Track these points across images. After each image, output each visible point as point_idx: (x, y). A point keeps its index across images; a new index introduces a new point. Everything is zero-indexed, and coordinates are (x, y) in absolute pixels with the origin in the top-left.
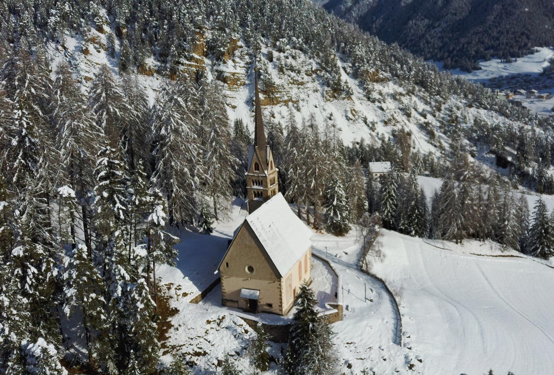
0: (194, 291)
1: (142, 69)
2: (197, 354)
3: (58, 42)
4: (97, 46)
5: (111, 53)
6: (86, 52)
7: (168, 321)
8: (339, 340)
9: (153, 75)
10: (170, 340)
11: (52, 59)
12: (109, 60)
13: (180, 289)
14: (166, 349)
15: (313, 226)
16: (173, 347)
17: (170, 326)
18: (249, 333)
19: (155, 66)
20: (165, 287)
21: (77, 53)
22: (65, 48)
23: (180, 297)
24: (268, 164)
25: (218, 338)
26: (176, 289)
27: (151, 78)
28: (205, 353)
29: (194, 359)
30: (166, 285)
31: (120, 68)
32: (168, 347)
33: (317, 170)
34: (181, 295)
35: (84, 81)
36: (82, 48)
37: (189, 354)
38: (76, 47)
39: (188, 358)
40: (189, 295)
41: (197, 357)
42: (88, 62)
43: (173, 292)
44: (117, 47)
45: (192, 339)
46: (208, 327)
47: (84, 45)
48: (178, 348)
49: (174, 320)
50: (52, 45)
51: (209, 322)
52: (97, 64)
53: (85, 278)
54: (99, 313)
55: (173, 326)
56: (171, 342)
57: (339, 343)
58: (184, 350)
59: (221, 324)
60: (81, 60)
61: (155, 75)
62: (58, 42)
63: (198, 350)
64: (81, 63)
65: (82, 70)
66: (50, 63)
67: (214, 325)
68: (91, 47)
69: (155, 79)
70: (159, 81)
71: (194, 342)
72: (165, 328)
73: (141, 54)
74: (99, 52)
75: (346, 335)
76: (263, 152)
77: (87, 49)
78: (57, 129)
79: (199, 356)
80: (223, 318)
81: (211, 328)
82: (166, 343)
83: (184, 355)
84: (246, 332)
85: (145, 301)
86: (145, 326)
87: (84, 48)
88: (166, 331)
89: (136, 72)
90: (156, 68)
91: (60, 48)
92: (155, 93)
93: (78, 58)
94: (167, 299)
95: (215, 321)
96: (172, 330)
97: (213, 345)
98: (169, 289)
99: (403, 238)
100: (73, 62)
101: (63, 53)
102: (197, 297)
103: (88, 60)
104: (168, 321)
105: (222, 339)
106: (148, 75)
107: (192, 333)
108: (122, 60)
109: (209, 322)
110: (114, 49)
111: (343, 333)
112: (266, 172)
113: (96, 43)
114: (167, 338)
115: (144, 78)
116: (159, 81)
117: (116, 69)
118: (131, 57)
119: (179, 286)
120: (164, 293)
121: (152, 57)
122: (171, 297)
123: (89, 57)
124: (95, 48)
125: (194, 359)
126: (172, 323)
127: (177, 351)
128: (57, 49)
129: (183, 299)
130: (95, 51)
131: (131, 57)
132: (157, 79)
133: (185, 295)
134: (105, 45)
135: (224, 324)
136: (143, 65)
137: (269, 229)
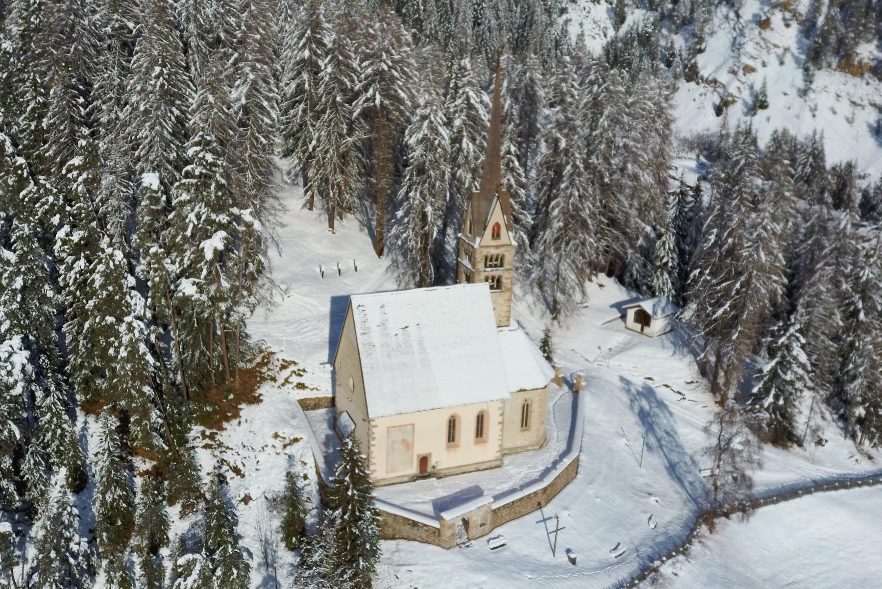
0: (323, 390)
1: (848, 64)
2: (237, 471)
3: (733, 5)
4: (788, 15)
5: (808, 28)
6: (764, 24)
7: (239, 407)
8: (408, 575)
9: (862, 75)
10: (224, 433)
11: (712, 34)
12: (799, 42)
13: (301, 375)
14: (210, 442)
15: (719, 399)
16: (220, 445)
17: (236, 415)
18: (307, 482)
19: (873, 59)
20: (279, 364)
21: (750, 26)
22: (738, 16)
23: (290, 386)
24: (485, 227)
25: (269, 465)
26: (294, 372)
27: (857, 80)
28: (243, 476)
29: (230, 475)
30: (283, 360)
31: (808, 55)
32: (215, 441)
33: (738, 286)
34: (295, 384)
35: (741, 72)
36: (760, 17)
37: (228, 465)
38: (755, 16)
39: (225, 468)
40: (307, 390)
41: (234, 475)
42: (762, 43)
43: (286, 373)
44: (821, 21)
45: (244, 446)
46: (271, 441)
47: (765, 13)
48: (223, 449)
49: (246, 410)
50: (723, 9)
51: (276, 436)
52: (776, 46)
53: (105, 293)
54: (110, 345)
55: (240, 417)
56: (222, 437)
57: (403, 579)
58: (228, 456)
59: (288, 447)
60: (752, 36)
61: (867, 75)
62: (733, 5)
63: (240, 466)
64: (750, 43)
65: (746, 54)
66: (707, 38)
67: (278, 443)
68: (777, 18)
69: (864, 82)
70: (869, 87)
71: (244, 453)
72: (229, 414)
73: (853, 35)
74: (788, 26)
75: (424, 575)
76: (484, 203)
77: (768, 20)
78: (174, 101)
79: (237, 475)
80: (296, 440)
81: (274, 446)
82: (217, 434)
83: (223, 461)
84: (305, 477)
85: (129, 349)
86: (127, 383)
87: (764, 18)
88: (228, 419)
89: (834, 66)
90: (873, 64)
91: (732, 15)
92: (851, 109)
93: (747, 34)
94: (263, 379)
95: (284, 438)
96: (235, 422)
97: (257, 470)
98: (283, 367)
99: (841, 503)
100: (739, 40)
101: (732, 23)
102: (320, 399)
103: (764, 39)
104: (239, 407)
105: (272, 468)
106: (854, 74)
107: (250, 438)
108: (816, 42)
109: (276, 436)
110: (814, 24)
111: (424, 568)
112: (478, 239)
113: (790, 11)
114: (222, 429)
115: (843, 79)
116: (870, 89)
117: (803, 57)
118: (833, 39)
119: (304, 371)
120: (269, 370)
121: (875, 42)
122: (274, 379)
123: (767, 34)
124: (784, 19)
125: (230, 475)
126: (241, 413)
127: (221, 452)
128: (727, 17)
129: (291, 391)
130: (782, 24)
131: (833, 39)
132: (868, 84)
133: (301, 386)
134: (801, 15)
135: (289, 450)
136: (850, 55)
137: (400, 332)
